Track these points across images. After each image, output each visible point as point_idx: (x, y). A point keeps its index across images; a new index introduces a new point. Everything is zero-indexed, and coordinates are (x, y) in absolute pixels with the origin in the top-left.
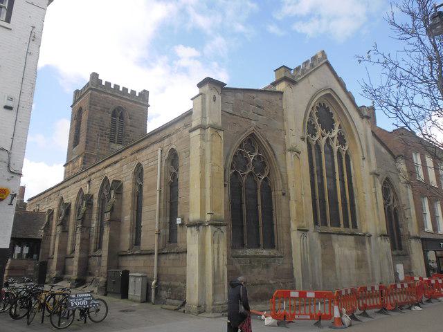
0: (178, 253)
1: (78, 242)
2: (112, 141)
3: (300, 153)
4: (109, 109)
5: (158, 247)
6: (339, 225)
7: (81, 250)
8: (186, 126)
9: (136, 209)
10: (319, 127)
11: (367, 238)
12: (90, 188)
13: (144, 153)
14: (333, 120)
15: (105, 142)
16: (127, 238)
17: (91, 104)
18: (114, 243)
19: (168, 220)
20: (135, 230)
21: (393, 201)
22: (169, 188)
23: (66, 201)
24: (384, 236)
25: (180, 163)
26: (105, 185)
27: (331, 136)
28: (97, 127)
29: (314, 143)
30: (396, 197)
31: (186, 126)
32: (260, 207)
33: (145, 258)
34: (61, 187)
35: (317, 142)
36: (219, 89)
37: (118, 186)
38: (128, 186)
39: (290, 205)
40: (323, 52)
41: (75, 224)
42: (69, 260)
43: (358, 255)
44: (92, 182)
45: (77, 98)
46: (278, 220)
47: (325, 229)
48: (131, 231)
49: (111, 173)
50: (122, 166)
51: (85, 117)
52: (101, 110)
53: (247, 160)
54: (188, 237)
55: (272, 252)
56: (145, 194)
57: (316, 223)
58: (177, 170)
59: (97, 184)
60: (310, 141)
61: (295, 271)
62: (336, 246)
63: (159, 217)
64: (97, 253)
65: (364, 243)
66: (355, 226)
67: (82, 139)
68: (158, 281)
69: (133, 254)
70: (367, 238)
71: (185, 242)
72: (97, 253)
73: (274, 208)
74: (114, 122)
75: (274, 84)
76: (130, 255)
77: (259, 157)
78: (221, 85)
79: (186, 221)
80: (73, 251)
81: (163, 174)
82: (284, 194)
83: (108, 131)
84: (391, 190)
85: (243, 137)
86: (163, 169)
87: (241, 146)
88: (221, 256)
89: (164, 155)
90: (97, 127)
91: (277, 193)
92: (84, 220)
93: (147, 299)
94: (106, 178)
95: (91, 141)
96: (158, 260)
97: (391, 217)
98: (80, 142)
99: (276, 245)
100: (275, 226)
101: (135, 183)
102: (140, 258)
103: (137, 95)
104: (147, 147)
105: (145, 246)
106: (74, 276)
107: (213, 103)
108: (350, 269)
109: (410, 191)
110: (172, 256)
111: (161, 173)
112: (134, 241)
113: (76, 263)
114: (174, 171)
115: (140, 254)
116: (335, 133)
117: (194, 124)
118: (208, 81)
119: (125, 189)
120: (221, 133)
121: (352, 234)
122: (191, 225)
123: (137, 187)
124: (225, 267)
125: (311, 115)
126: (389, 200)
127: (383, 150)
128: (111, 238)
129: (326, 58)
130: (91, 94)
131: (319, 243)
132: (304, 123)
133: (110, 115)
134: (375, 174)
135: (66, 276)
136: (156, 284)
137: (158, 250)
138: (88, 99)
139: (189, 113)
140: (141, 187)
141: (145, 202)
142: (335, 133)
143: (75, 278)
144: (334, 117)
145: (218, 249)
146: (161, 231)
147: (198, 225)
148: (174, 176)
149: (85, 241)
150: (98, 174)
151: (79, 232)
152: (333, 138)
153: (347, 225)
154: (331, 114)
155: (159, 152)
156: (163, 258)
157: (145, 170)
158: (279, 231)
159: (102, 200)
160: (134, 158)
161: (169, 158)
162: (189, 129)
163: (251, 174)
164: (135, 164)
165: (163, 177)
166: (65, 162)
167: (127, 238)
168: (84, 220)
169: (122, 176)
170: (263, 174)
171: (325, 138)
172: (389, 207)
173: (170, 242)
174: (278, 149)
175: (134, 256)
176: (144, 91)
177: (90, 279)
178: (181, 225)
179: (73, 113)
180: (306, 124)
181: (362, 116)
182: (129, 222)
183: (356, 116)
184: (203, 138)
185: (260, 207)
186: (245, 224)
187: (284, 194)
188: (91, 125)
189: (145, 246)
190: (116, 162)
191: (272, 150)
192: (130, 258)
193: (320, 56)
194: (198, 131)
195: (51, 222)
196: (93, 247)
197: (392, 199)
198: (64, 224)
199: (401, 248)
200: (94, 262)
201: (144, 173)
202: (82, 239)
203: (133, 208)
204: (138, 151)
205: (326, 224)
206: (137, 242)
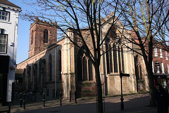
7: (35, 82)
16: (48, 78)
45: (31, 27)
80: (32, 82)
92: (35, 72)
101: (49, 60)
105: (53, 81)
119: (46, 62)
128: (43, 78)
130: (36, 25)
140: (51, 61)
146: (57, 76)
155: (56, 50)
156: (58, 84)
161: (59, 52)
164: (49, 54)
165: (57, 59)
167: (48, 78)
189: (53, 81)
192: (49, 84)
196: (38, 81)
206: (51, 79)
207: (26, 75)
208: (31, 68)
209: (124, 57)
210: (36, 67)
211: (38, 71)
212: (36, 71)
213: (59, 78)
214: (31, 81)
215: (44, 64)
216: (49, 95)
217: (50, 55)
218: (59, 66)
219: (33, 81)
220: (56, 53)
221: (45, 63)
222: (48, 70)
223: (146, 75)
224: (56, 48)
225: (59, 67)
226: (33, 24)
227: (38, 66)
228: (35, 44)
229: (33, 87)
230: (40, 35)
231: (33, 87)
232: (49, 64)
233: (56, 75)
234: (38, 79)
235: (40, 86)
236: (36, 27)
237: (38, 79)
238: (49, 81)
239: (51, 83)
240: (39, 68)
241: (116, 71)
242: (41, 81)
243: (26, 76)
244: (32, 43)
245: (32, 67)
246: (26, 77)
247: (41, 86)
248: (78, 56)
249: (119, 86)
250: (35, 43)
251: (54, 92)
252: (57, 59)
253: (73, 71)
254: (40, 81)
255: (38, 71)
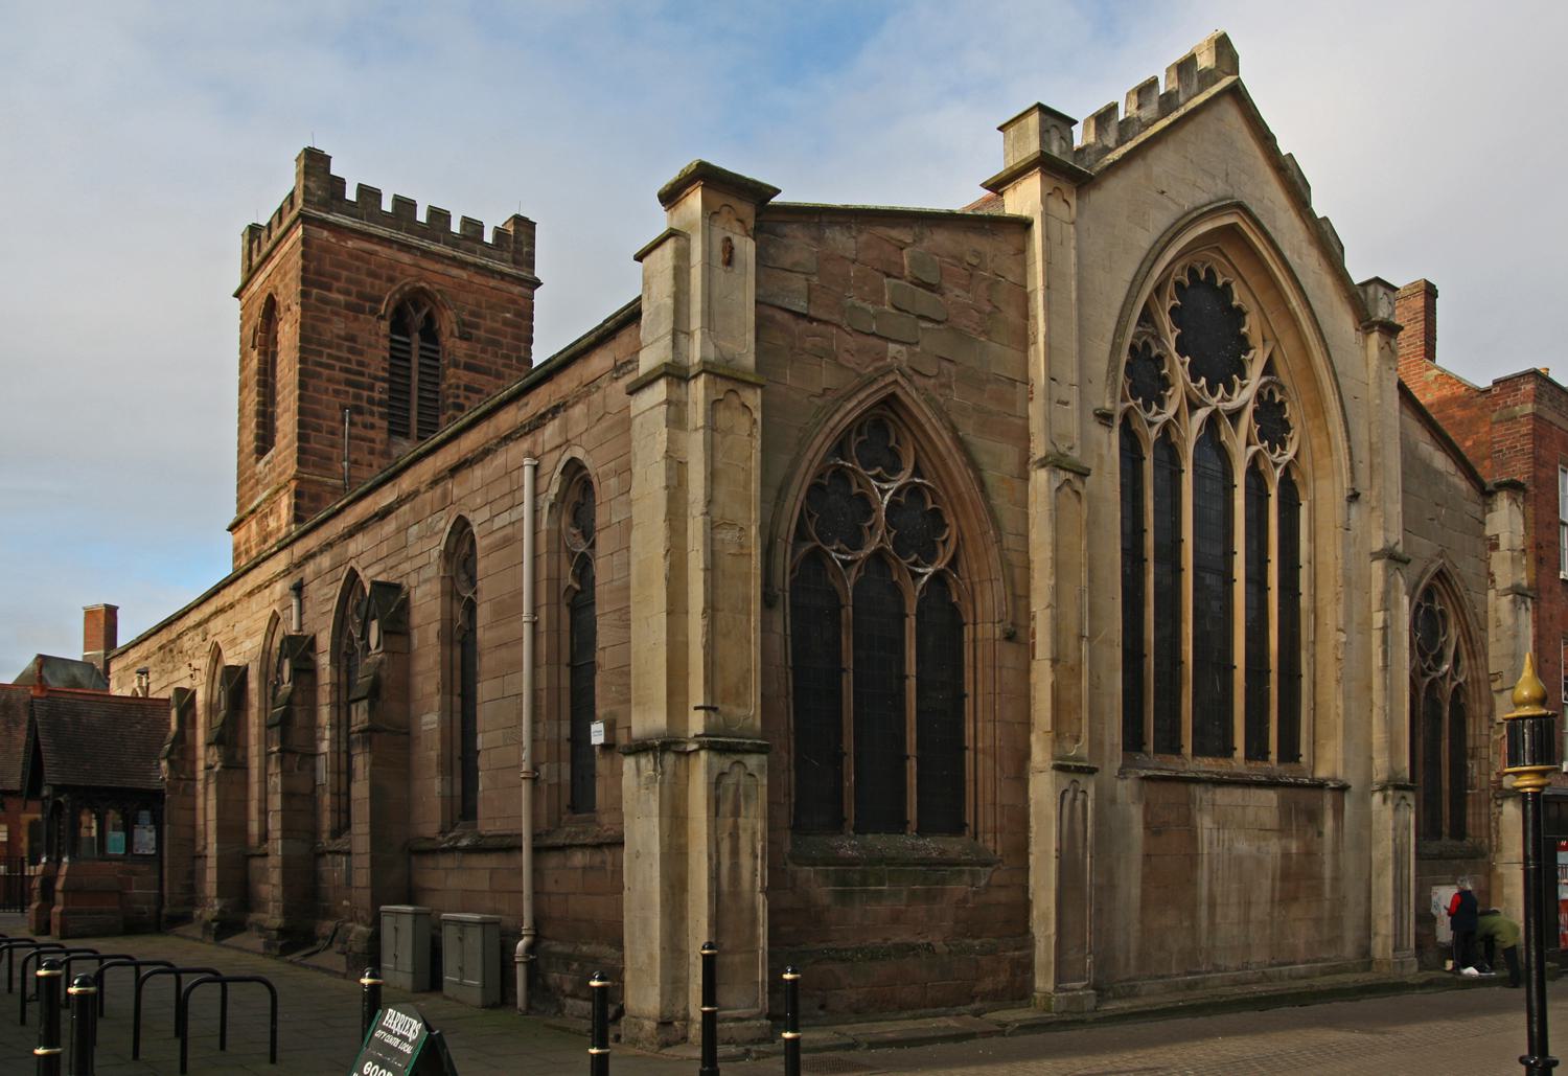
0: (598, 846)
1: (276, 802)
2: (398, 429)
3: (1083, 474)
4: (379, 300)
5: (535, 816)
6: (1227, 751)
7: (287, 831)
8: (619, 369)
9: (458, 690)
10: (1179, 369)
11: (1328, 799)
12: (301, 613)
13: (478, 473)
14: (1243, 339)
15: (371, 434)
16: (432, 789)
17: (311, 279)
18: (390, 810)
19: (566, 730)
20: (458, 765)
21: (1457, 660)
22: (565, 612)
23: (231, 659)
24: (1397, 788)
25: (600, 519)
26: (352, 602)
27: (1229, 406)
28: (337, 374)
29: (1153, 434)
30: (1474, 644)
31: (619, 369)
32: (848, 681)
33: (491, 861)
34: (208, 609)
35: (1166, 428)
36: (747, 210)
37: (390, 603)
38: (427, 603)
39: (1034, 677)
40: (1223, 45)
41: (266, 741)
42: (256, 863)
43: (1286, 855)
44: (311, 589)
45: (256, 259)
46: (980, 731)
47: (1172, 765)
48: (445, 768)
49: (369, 557)
50: (402, 529)
51: (288, 333)
52: (348, 306)
53: (865, 505)
54: (627, 795)
55: (954, 846)
56: (484, 636)
57: (1133, 740)
58: (593, 546)
59: (325, 596)
60: (1135, 426)
61: (1035, 913)
62: (1205, 823)
63: (535, 720)
64: (339, 844)
65: (1313, 817)
66: (1290, 752)
67: (286, 424)
68: (537, 938)
69: (453, 849)
70: (1328, 799)
71: (617, 808)
72: (339, 844)
73: (969, 689)
74: (398, 354)
75: (998, 186)
76: (444, 851)
77: (914, 491)
78: (759, 194)
79: (622, 739)
80: (264, 836)
81: (544, 558)
82: (1010, 637)
83: (380, 391)
84: (1452, 621)
85: (851, 409)
86: (543, 537)
87: (840, 448)
88: (745, 861)
89: (543, 483)
90: (337, 374)
91: (983, 630)
92: (291, 726)
93: (500, 995)
94: (353, 575)
95: (318, 429)
96: (536, 871)
97: (1436, 718)
98: (279, 437)
99: (969, 819)
100: (969, 755)
101: (450, 593)
102: (475, 861)
103: (488, 238)
104: (485, 453)
105: (489, 823)
106: (272, 916)
107: (719, 269)
108: (1249, 904)
109: (1526, 620)
110: (579, 859)
111: (535, 557)
112: (458, 802)
113: (275, 877)
114: (582, 548)
115: (477, 849)
116: (1245, 396)
117: (648, 361)
118: (706, 176)
119: (416, 618)
120: (753, 398)
121: (1271, 783)
122: (640, 748)
123: (458, 610)
124: (760, 898)
125: (1147, 316)
126: (1439, 659)
127: (1441, 461)
128: (376, 792)
129: (1234, 68)
130: (305, 241)
131: (1136, 813)
132: (1115, 349)
133: (385, 326)
134: (1391, 557)
135: (254, 917)
136: (530, 949)
137: (535, 836)
138: (297, 260)
139: (631, 316)
140: (471, 607)
141: (486, 663)
142: (1245, 396)
143: (278, 922)
144: (1252, 326)
145: (735, 836)
146: (543, 769)
147: (667, 746)
148: (584, 567)
149: (300, 803)
150: (325, 561)
151: (274, 768)
152: (1235, 415)
153: (1256, 750)
154: (1239, 315)
155: (527, 472)
156: (553, 860)
157: (482, 544)
158: (982, 770)
159: (345, 654)
160: (445, 496)
161: (562, 496)
162: (628, 379)
163: (879, 555)
164: (444, 524)
165: (543, 573)
166: (232, 516)
167: (432, 789)
168: (291, 726)
169: (406, 567)
170: (930, 558)
171: (1202, 414)
172: (1433, 684)
173: (574, 808)
174: (997, 457)
175: (458, 855)
176: (661, 201)
177: (327, 926)
178: (607, 747)
179: (245, 319)
180: (1124, 357)
181: (1366, 322)
182: (437, 736)
183: (1340, 322)
184: (676, 416)
185: (848, 681)
186: (848, 744)
187: (1010, 637)
188: (311, 367)
189: (489, 823)
190: (383, 514)
191: (973, 464)
192: (446, 861)
193: (1206, 61)
194: (660, 390)
195: (188, 732)
196: (327, 821)
197: (1450, 653)
198: (229, 737)
199: (1459, 831)
200: (333, 871)
201: (479, 555)
202: (287, 795)
203: (446, 687)
204: (454, 470)
205: (1175, 748)
206: (465, 806)
207: (201, 765)
208: (253, 684)
209: (1304, 587)
210: (305, 670)
211: (325, 714)
212: (299, 717)
213: (566, 799)
214: (254, 827)
215: (385, 632)
216: (450, 978)
217: (462, 526)
218: (566, 657)
219: (275, 824)
220: (526, 509)
221: (397, 623)
222: (437, 700)
223: (1394, 785)
224: (525, 444)
225: (566, 673)
226: (276, 233)
227: (324, 660)
228: (301, 450)
229: (271, 885)
230: (351, 350)
231: (271, 885)
232: (441, 635)
233: (525, 755)
234: (327, 799)
235: (349, 878)
236: (304, 255)
237: (327, 799)
238: (443, 832)
239: (467, 850)
240: (336, 686)
241: (1215, 740)
242: (361, 828)
243: (201, 775)
244: (265, 440)
245: (264, 675)
246: (200, 786)
247: (362, 877)
248: (801, 534)
249: (1234, 899)
250: (302, 438)
251: (506, 950)
252: (543, 573)
253: (749, 713)
254: (348, 826)
255: (325, 714)
